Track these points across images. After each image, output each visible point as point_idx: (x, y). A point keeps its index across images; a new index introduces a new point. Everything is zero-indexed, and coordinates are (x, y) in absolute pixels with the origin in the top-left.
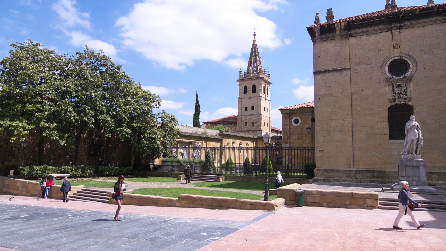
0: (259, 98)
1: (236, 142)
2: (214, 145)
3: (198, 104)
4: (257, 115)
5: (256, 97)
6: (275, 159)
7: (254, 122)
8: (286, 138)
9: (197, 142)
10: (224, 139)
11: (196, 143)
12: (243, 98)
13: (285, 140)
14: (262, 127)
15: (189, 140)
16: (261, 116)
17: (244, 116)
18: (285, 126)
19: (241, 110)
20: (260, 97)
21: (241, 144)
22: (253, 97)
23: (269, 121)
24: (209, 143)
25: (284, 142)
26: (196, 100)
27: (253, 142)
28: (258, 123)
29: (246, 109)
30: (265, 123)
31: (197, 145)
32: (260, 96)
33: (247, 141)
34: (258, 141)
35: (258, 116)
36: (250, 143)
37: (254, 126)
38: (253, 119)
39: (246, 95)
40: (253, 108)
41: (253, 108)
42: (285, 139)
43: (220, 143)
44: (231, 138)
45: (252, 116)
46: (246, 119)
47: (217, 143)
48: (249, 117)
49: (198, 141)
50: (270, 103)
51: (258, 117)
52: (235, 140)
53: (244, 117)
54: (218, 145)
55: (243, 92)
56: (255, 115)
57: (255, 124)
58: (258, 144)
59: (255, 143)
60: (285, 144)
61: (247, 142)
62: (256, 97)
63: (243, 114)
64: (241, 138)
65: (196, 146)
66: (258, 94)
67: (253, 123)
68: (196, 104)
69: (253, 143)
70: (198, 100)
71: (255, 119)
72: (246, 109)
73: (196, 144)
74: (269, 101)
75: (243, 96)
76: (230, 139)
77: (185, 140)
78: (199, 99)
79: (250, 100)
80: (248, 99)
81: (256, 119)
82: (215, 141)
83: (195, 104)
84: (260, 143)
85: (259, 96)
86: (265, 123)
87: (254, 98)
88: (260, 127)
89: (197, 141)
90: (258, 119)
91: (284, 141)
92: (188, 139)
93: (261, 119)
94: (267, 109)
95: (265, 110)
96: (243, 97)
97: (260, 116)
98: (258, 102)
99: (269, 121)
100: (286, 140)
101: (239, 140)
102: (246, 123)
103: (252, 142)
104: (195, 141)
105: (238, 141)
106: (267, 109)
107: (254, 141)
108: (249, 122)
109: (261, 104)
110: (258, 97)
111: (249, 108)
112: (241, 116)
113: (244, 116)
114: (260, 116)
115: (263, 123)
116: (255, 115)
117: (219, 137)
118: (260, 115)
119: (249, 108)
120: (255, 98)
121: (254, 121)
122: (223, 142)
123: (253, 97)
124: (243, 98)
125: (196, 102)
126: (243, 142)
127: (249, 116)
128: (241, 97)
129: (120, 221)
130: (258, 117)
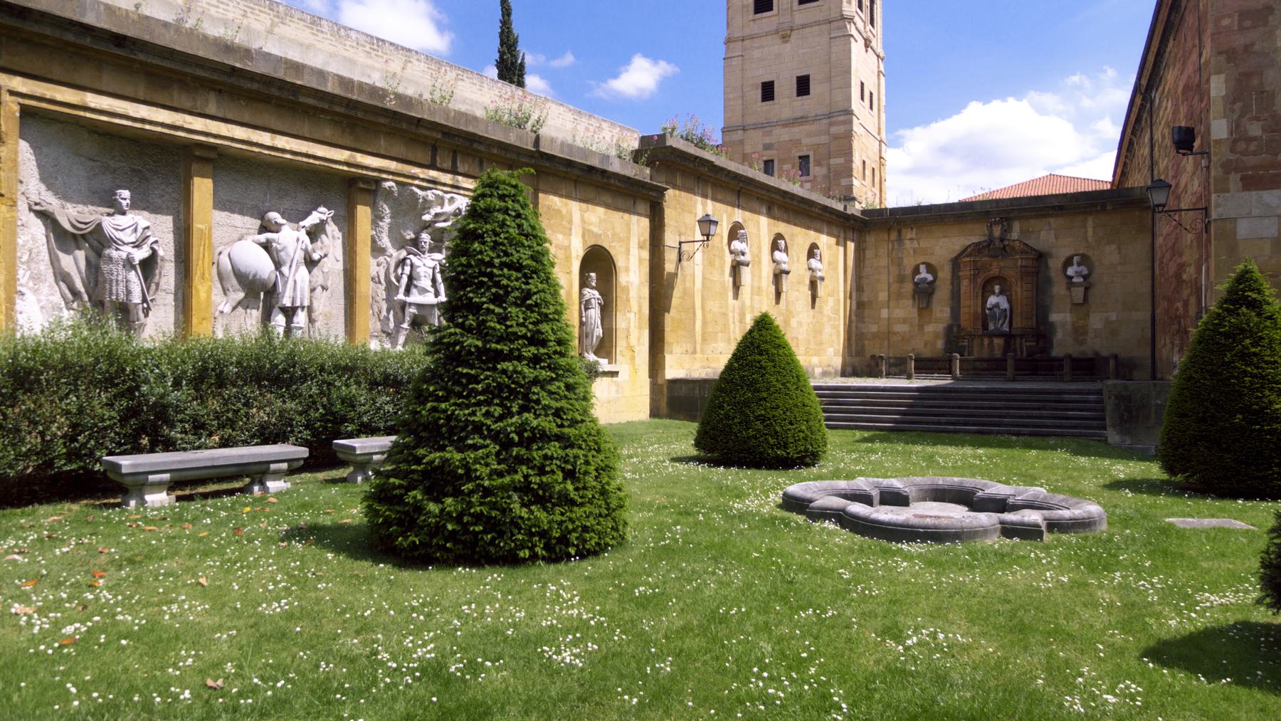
0: (839, 28)
1: (749, 229)
2: (595, 230)
3: (515, 57)
4: (829, 116)
5: (818, 23)
6: (986, 341)
7: (811, 159)
8: (1257, 132)
9: (434, 182)
10: (671, 194)
11: (430, 195)
12: (752, 37)
13: (1245, 153)
14: (855, 182)
15: (343, 155)
16: (851, 122)
17: (756, 127)
18: (1242, 29)
19: (740, 102)
20: (841, 23)
21: (782, 243)
22: (804, 26)
23: (881, 158)
24: (559, 211)
25: (1234, 179)
26: (502, 34)
27: (841, 240)
28: (833, 161)
29: (768, 91)
30: (864, 162)
31: (438, 210)
32: (843, 18)
33: (812, 233)
34: (871, 239)
35: (831, 124)
36: (829, 247)
37: (811, 177)
38: (808, 139)
39: (764, 21)
40: (803, 86)
41: (803, 86)
42: (1242, 146)
43: (645, 223)
44: (719, 197)
45: (801, 124)
46: (767, 147)
47: (626, 216)
48: (783, 135)
49: (447, 178)
50: (882, 69)
51: (834, 130)
52: (747, 213)
53: (759, 133)
54: (629, 231)
55: (747, 6)
56: (816, 119)
57: (817, 168)
58: (869, 254)
59: (851, 246)
60: (1246, 194)
61: (813, 236)
62: (818, 23)
63: (750, 120)
64: (780, 207)
65: (427, 217)
66: (830, 9)
67: (804, 159)
68: (502, 54)
69: (841, 249)
70: (510, 31)
71: (815, 140)
72: (768, 91)
73: (427, 205)
74: (878, 56)
75: (753, 29)
76: (714, 199)
77: (282, 142)
78: (517, 28)
79: (788, 46)
80: (779, 41)
81: (824, 139)
82: (607, 198)
83: (497, 56)
84: (883, 251)
85: (834, 15)
86: (864, 162)
87: (808, 30)
88: (844, 182)
89: (433, 174)
90: (836, 137)
91: (1228, 167)
92: (328, 133)
93: (848, 135)
94: (871, 94)
95: (862, 98)
96: (747, 31)
97: (844, 123)
98: (834, 49)
99: (881, 158)
100: (1251, 160)
101: (770, 215)
102: (804, 159)
103: (838, 244)
104: (416, 171)
105: (764, 221)
106: (871, 94)
107: (850, 234)
108: (782, 161)
109: (849, 59)
110: (834, 25)
111: (785, 88)
112: (740, 132)
113: (756, 127)
114: (844, 123)
115: (857, 164)
116: (816, 119)
117: (643, 173)
118: (842, 118)
119: (785, 88)
120: (816, 29)
121: (811, 154)
122: (670, 214)
123: (804, 26)
124: (752, 37)
125: (502, 44)
126: (792, 235)
127: (785, 126)
128: (738, 34)
129: (731, 294)
130: (834, 130)
